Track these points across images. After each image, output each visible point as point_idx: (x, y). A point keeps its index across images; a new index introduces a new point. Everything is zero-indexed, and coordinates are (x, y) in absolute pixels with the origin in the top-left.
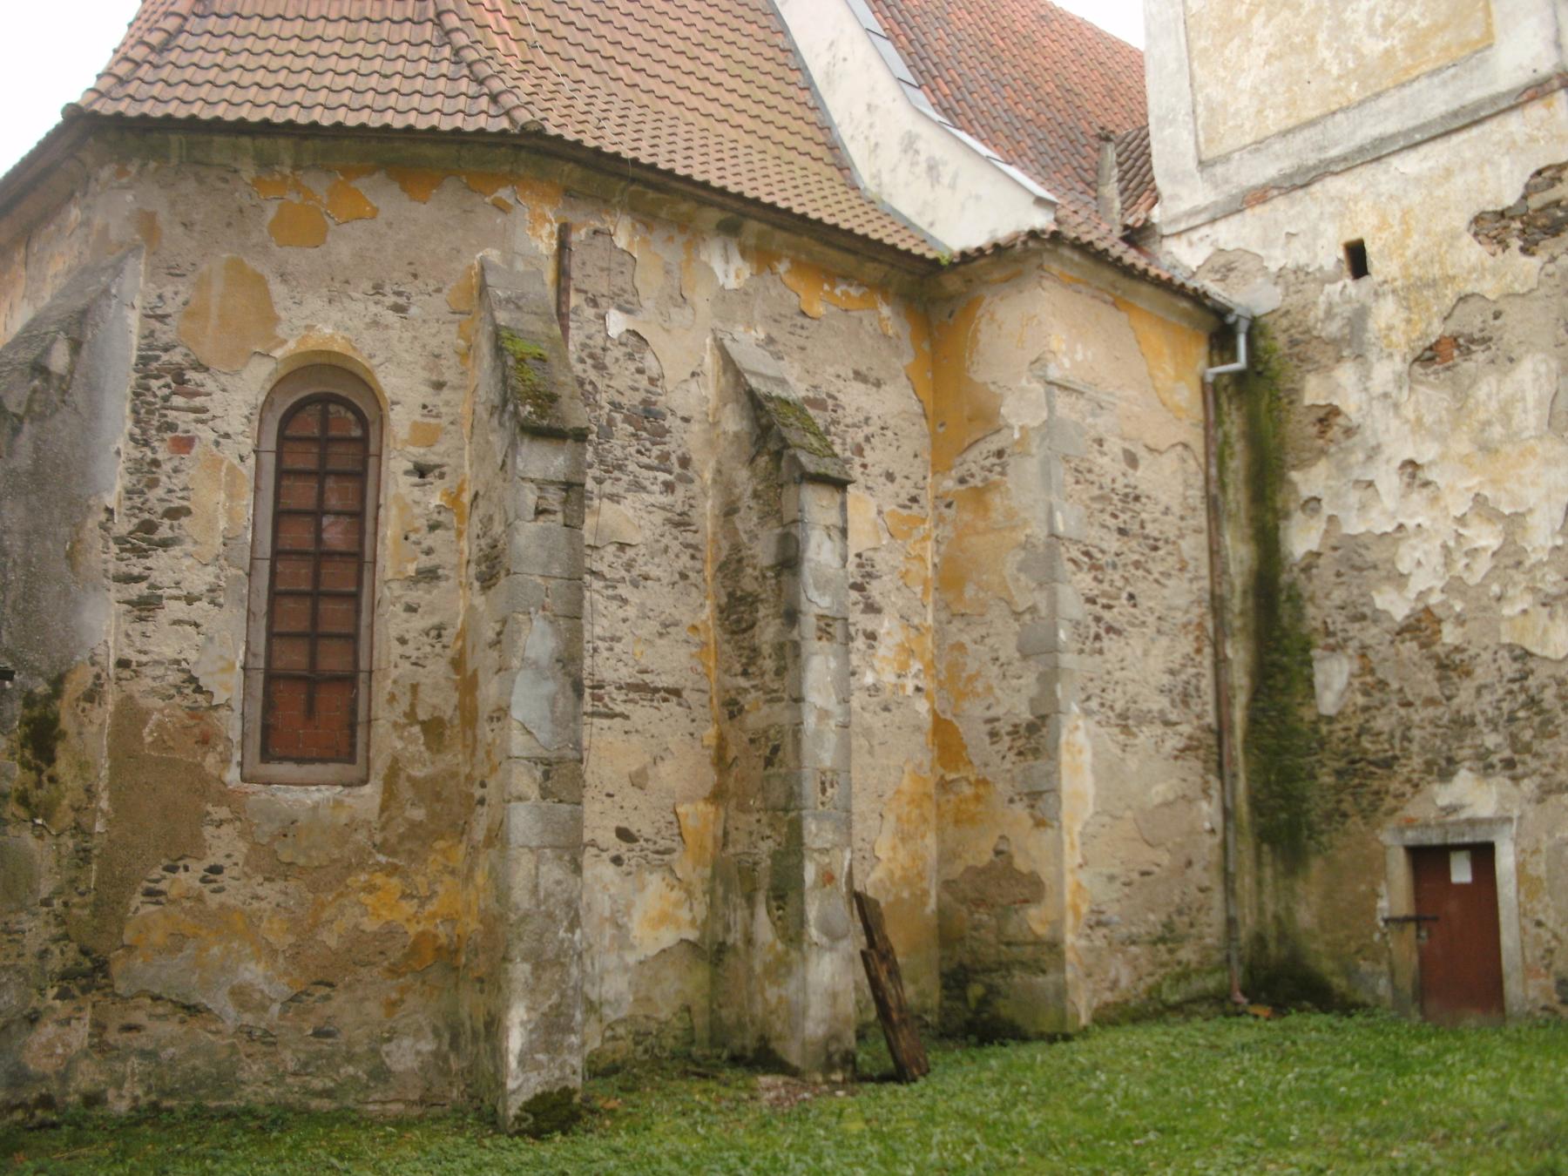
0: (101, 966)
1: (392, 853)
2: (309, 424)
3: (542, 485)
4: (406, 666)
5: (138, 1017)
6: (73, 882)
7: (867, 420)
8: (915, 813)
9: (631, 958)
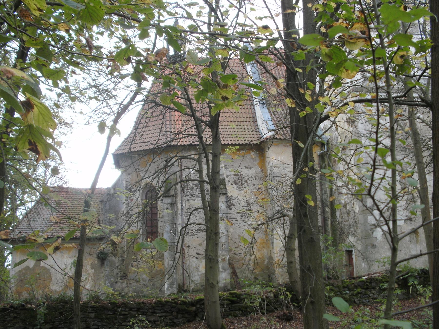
0: (127, 275)
1: (161, 258)
2: (149, 195)
3: (167, 204)
4: (161, 230)
5: (131, 282)
6: (122, 264)
7: (248, 176)
8: (261, 246)
9: (200, 273)
